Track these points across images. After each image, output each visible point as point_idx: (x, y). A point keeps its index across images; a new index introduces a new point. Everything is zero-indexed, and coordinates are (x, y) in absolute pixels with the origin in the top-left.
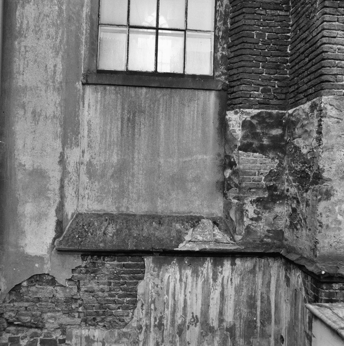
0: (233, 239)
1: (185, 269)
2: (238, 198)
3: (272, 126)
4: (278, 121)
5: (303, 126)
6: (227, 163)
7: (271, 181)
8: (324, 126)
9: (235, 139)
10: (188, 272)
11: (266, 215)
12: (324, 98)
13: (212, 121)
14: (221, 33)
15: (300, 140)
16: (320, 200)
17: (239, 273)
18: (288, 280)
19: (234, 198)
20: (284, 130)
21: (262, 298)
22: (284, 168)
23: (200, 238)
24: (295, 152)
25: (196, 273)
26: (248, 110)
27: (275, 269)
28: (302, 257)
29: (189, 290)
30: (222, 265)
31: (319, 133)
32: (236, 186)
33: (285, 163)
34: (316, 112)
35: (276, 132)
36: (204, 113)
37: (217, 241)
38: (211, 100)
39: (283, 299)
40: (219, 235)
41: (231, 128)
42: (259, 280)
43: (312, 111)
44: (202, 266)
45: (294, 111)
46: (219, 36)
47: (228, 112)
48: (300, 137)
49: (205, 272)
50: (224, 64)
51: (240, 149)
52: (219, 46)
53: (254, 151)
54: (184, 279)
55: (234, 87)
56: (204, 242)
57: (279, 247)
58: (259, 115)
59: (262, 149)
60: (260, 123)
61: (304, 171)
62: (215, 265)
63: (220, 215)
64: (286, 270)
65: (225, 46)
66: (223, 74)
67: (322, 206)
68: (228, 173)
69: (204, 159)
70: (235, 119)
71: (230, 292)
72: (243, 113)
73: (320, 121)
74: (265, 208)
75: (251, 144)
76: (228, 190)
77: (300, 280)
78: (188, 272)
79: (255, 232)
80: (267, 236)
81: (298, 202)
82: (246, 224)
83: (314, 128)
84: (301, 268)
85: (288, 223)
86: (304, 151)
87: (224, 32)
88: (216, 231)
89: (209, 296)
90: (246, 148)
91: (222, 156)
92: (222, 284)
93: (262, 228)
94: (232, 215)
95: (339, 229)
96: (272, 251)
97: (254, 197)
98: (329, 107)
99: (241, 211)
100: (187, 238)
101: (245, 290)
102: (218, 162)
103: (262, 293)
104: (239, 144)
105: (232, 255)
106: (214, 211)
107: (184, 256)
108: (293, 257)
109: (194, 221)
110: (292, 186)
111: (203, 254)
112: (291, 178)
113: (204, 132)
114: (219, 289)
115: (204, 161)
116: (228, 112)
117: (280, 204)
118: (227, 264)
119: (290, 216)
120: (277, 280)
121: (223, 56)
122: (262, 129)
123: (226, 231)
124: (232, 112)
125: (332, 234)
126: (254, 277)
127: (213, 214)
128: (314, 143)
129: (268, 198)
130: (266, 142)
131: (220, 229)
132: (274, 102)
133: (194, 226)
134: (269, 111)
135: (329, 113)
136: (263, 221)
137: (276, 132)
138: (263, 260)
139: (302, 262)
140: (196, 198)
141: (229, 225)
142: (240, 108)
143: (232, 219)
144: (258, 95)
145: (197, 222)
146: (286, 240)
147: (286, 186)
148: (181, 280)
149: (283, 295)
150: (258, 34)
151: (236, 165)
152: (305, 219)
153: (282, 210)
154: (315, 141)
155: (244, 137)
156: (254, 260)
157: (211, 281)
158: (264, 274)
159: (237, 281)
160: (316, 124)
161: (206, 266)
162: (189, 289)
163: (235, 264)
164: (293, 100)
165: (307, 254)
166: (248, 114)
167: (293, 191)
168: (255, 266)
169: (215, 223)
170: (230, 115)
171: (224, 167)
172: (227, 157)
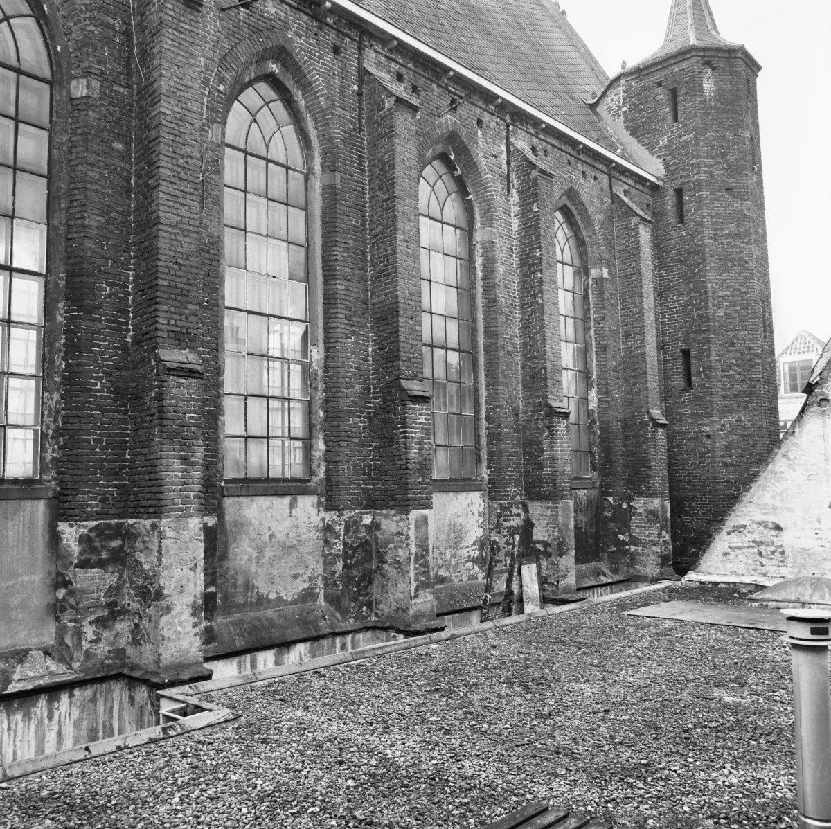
0: (70, 668)
1: (14, 714)
2: (75, 621)
3: (111, 538)
4: (118, 532)
5: (144, 542)
6: (60, 581)
7: (110, 596)
8: (163, 547)
9: (70, 555)
10: (19, 717)
11: (106, 634)
12: (164, 521)
13: (40, 536)
14: (50, 432)
15: (141, 554)
16: (162, 615)
17: (78, 704)
18: (132, 699)
19: (70, 621)
20: (123, 540)
21: (104, 726)
22: (124, 582)
23: (31, 674)
24: (136, 566)
25: (27, 716)
26: (85, 523)
27: (118, 691)
28: (147, 672)
29: (20, 738)
30: (58, 700)
31: (160, 553)
32: (73, 607)
33: (125, 576)
34: (156, 533)
35: (115, 544)
36: (31, 526)
37: (52, 674)
38: (39, 510)
39: (127, 722)
40: (53, 666)
41: (65, 542)
42: (101, 708)
43: (153, 530)
44: (34, 706)
45: (135, 523)
46: (48, 435)
47: (59, 523)
48: (141, 551)
49: (38, 712)
50: (56, 467)
51: (77, 566)
52: (48, 446)
53: (93, 567)
54: (13, 727)
55: (67, 495)
56: (37, 678)
57: (122, 667)
58: (97, 526)
59: (101, 564)
60: (98, 536)
61: (146, 587)
62: (50, 702)
63: (51, 643)
64: (130, 690)
65: (56, 447)
66: (54, 479)
67: (164, 619)
68: (61, 593)
69: (32, 581)
70: (70, 534)
71: (69, 729)
72: (79, 526)
73: (160, 542)
74: (105, 627)
75: (89, 559)
76: (62, 612)
77: (146, 695)
78: (19, 717)
79: (95, 655)
80: (108, 658)
81: (141, 617)
82: (85, 648)
83: (154, 547)
84: (145, 682)
85: (130, 640)
86: (146, 567)
87: (54, 431)
88: (49, 662)
89: (43, 739)
90: (83, 564)
91: (54, 574)
92: (59, 721)
93: (102, 649)
94: (68, 641)
95: (179, 639)
96: (114, 672)
97: (93, 617)
98: (168, 529)
99: (79, 634)
100: (16, 677)
101: (85, 723)
102: (48, 581)
103: (104, 722)
104: (76, 561)
105: (69, 686)
106: (44, 639)
107: (13, 699)
108: (137, 674)
109: (20, 656)
110: (133, 601)
111: (37, 692)
112: (132, 592)
113: (31, 548)
114: (56, 728)
115: (31, 582)
116: (59, 523)
117: (121, 620)
118: (64, 698)
119: (132, 632)
120: (120, 704)
121: (53, 459)
122: (100, 541)
123: (61, 660)
124: (66, 524)
125: (172, 644)
126: (95, 705)
127: (43, 643)
128: (155, 562)
129: (108, 616)
130: (104, 555)
131: (53, 659)
132: (114, 511)
133: (21, 662)
134: (108, 521)
135: (168, 535)
136: (103, 641)
137: (115, 544)
138: (104, 685)
139: (147, 677)
140: (22, 627)
141: (64, 652)
142: (76, 521)
143: (67, 646)
144: (95, 505)
145: (25, 656)
146: (129, 658)
147: (127, 600)
148: (9, 729)
149: (127, 718)
150: (95, 440)
151: (72, 584)
152: (148, 634)
153: (123, 626)
154: (155, 560)
155: (81, 553)
156: (95, 686)
157: (46, 721)
158: (106, 700)
159: (76, 714)
160: (157, 544)
161: (39, 705)
162: (19, 737)
163: (73, 696)
164: (133, 510)
165: (151, 668)
166: (85, 527)
167: (135, 605)
168: (95, 693)
169: (46, 653)
170: (63, 526)
171: (56, 587)
172: (63, 575)
